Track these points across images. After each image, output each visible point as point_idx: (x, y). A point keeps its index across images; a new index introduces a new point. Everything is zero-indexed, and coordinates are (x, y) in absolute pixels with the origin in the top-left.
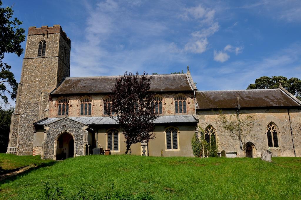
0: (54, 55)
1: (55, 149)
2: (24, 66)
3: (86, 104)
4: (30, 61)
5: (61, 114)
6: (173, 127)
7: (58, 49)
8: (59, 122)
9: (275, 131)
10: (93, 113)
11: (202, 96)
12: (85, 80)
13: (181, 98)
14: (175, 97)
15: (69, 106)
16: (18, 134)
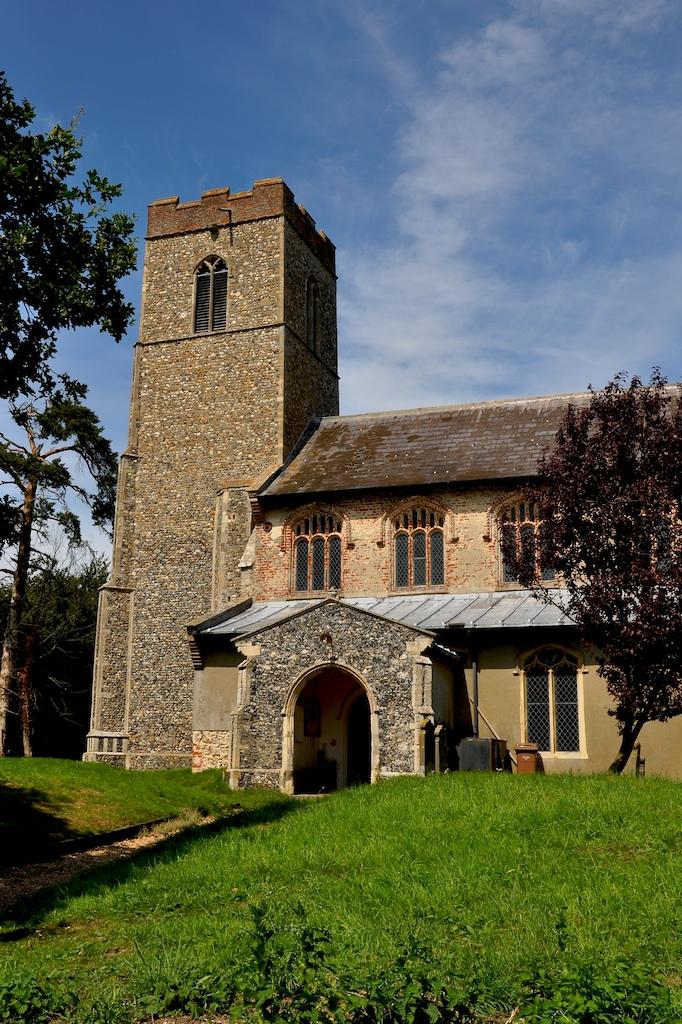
0: (267, 321)
1: (287, 743)
2: (141, 379)
3: (419, 535)
4: (163, 356)
5: (310, 582)
6: (560, 647)
7: (280, 292)
8: (302, 619)
10: (453, 574)
12: (412, 426)
15: (344, 545)
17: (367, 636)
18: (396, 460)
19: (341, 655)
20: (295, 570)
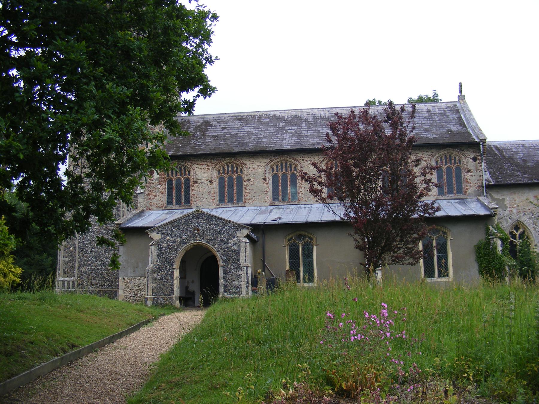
1: (176, 283)
10: (248, 197)
11: (496, 154)
12: (223, 122)
13: (451, 160)
14: (435, 157)
15: (192, 182)
16: (77, 249)
17: (217, 229)
18: (217, 139)
19: (204, 238)
20: (166, 195)
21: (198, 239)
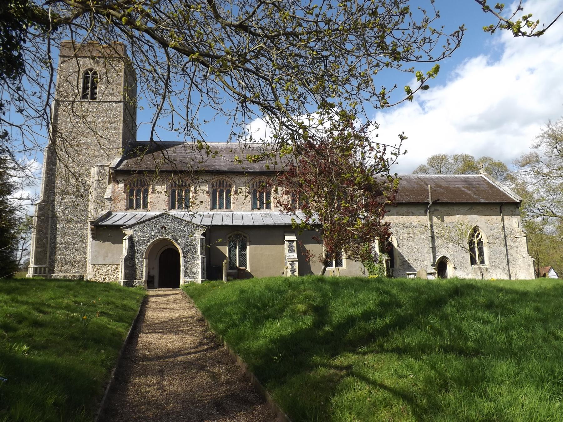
0: (115, 99)
6: (241, 233)
8: (152, 221)
9: (480, 240)
16: (49, 241)
21: (164, 235)
